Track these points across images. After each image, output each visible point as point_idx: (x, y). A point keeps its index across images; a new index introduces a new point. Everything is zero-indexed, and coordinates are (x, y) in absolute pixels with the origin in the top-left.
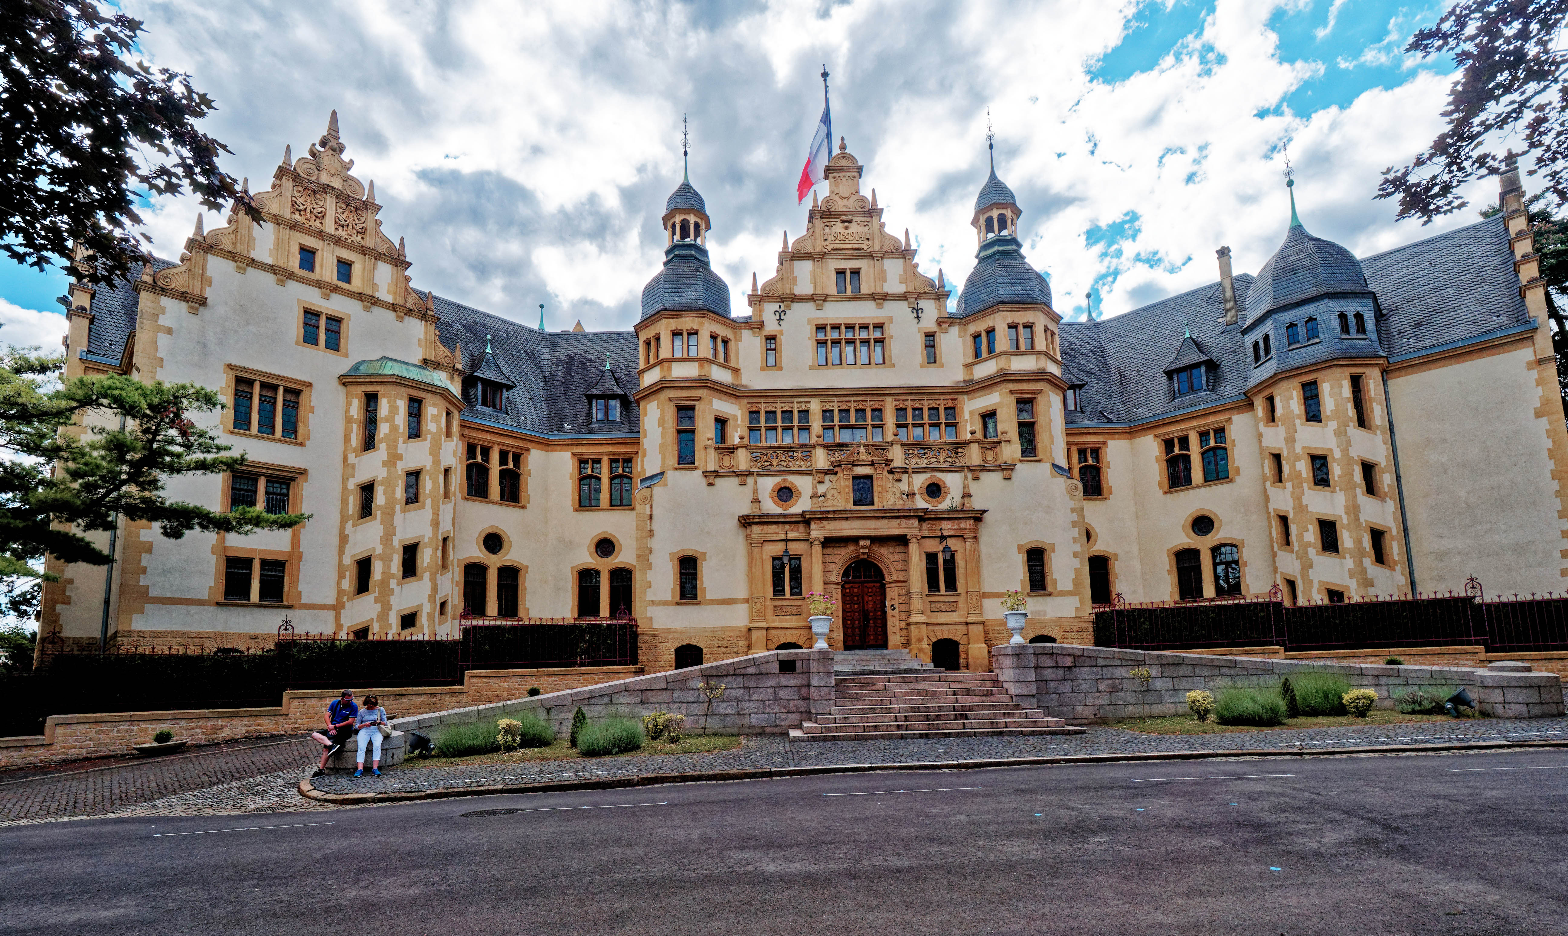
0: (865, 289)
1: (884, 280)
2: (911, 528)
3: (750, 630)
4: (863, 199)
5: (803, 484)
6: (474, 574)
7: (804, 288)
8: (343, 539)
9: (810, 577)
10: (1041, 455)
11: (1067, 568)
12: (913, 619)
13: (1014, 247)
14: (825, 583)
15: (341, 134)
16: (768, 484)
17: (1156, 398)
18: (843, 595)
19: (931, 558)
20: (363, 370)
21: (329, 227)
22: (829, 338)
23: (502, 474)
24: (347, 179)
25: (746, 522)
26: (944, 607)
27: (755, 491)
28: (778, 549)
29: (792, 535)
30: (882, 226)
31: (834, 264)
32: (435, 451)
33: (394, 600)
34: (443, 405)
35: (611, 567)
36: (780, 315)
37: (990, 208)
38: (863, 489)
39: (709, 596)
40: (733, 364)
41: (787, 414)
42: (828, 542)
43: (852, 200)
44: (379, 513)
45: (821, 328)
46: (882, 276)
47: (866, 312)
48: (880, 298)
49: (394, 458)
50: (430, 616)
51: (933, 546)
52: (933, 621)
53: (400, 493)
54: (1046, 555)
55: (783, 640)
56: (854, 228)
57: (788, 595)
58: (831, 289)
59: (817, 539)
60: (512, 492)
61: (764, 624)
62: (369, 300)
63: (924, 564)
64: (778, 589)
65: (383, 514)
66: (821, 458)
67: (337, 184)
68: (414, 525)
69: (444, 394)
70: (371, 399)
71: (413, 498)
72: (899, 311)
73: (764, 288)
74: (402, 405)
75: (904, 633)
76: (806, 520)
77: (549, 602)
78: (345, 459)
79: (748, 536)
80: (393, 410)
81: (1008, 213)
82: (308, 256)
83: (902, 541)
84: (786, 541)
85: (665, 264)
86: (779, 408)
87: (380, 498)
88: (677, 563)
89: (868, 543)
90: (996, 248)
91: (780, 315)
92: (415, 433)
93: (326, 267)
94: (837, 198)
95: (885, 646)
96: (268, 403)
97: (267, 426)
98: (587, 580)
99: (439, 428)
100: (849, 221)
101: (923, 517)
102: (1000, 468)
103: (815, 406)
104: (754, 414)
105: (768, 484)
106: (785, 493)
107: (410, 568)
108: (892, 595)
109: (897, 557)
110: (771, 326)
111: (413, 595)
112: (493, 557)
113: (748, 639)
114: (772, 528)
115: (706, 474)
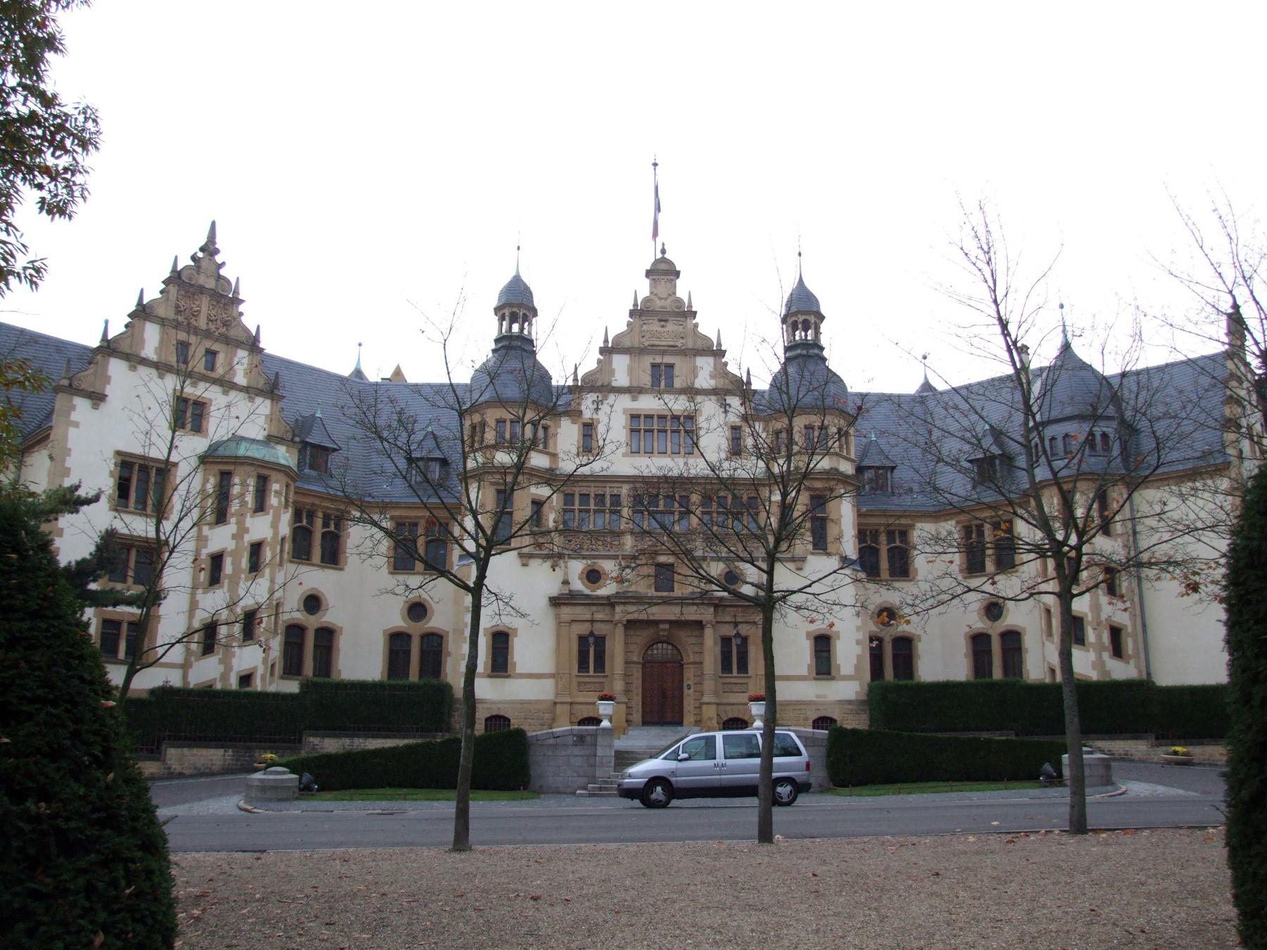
0: (678, 383)
1: (696, 377)
2: (707, 614)
3: (555, 703)
4: (680, 301)
5: (609, 566)
6: (294, 633)
7: (621, 379)
8: (193, 605)
9: (613, 656)
10: (831, 548)
11: (850, 652)
12: (706, 699)
13: (816, 351)
14: (626, 662)
15: (217, 240)
16: (577, 567)
17: (957, 484)
18: (644, 674)
19: (726, 641)
20: (221, 452)
21: (202, 323)
22: (643, 429)
23: (324, 535)
24: (219, 277)
25: (555, 602)
26: (735, 688)
27: (566, 574)
28: (584, 629)
29: (599, 616)
30: (696, 326)
31: (648, 360)
32: (275, 525)
33: (235, 662)
34: (284, 479)
35: (422, 632)
36: (598, 403)
37: (796, 314)
38: (664, 576)
39: (518, 671)
40: (551, 450)
41: (600, 498)
42: (631, 625)
43: (669, 301)
44: (226, 582)
45: (634, 417)
46: (694, 372)
47: (679, 405)
48: (691, 392)
49: (243, 530)
50: (263, 677)
51: (728, 631)
52: (725, 701)
53: (245, 563)
54: (832, 641)
55: (585, 715)
56: (670, 327)
57: (591, 673)
58: (646, 380)
59: (619, 622)
60: (333, 557)
61: (569, 700)
62: (227, 385)
63: (718, 649)
64: (583, 665)
65: (230, 582)
66: (629, 542)
67: (211, 284)
68: (256, 592)
69: (283, 470)
70: (225, 477)
71: (255, 567)
72: (709, 407)
73: (583, 380)
74: (252, 482)
75: (697, 711)
76: (609, 602)
77: (361, 662)
78: (629, 793)
79: (557, 616)
80: (243, 488)
81: (812, 319)
82: (183, 347)
83: (699, 625)
84: (592, 621)
85: (494, 351)
86: (592, 491)
87: (228, 567)
88: (490, 638)
89: (667, 626)
90: (799, 351)
91: (598, 403)
92: (260, 507)
93: (198, 363)
94: (656, 299)
95: (680, 723)
96: (144, 481)
97: (142, 503)
98: (397, 641)
99: (280, 502)
100: (666, 321)
101: (718, 605)
102: (793, 560)
103: (625, 490)
104: (568, 498)
105: (577, 567)
106: (593, 576)
107: (249, 633)
108: (689, 675)
109: (693, 640)
110: (587, 414)
111: (249, 658)
112: (312, 618)
113: (553, 712)
114: (578, 610)
115: (521, 556)
